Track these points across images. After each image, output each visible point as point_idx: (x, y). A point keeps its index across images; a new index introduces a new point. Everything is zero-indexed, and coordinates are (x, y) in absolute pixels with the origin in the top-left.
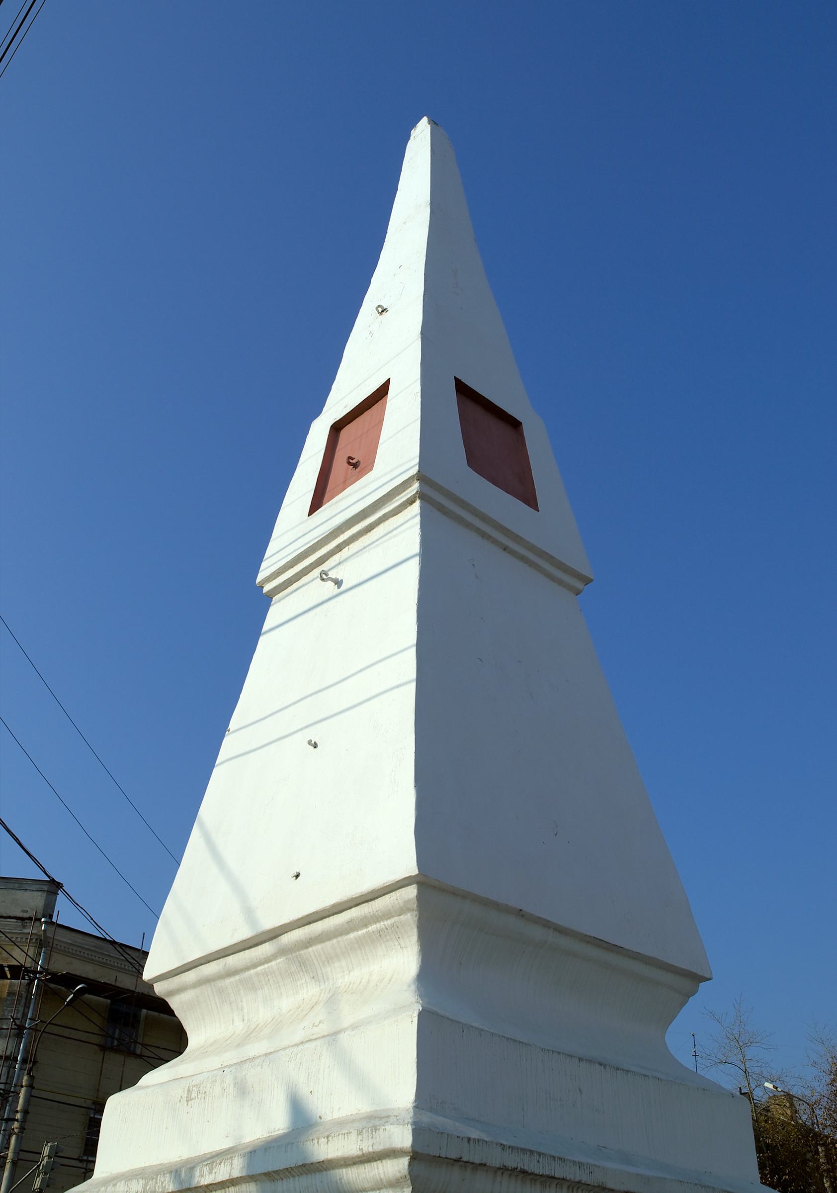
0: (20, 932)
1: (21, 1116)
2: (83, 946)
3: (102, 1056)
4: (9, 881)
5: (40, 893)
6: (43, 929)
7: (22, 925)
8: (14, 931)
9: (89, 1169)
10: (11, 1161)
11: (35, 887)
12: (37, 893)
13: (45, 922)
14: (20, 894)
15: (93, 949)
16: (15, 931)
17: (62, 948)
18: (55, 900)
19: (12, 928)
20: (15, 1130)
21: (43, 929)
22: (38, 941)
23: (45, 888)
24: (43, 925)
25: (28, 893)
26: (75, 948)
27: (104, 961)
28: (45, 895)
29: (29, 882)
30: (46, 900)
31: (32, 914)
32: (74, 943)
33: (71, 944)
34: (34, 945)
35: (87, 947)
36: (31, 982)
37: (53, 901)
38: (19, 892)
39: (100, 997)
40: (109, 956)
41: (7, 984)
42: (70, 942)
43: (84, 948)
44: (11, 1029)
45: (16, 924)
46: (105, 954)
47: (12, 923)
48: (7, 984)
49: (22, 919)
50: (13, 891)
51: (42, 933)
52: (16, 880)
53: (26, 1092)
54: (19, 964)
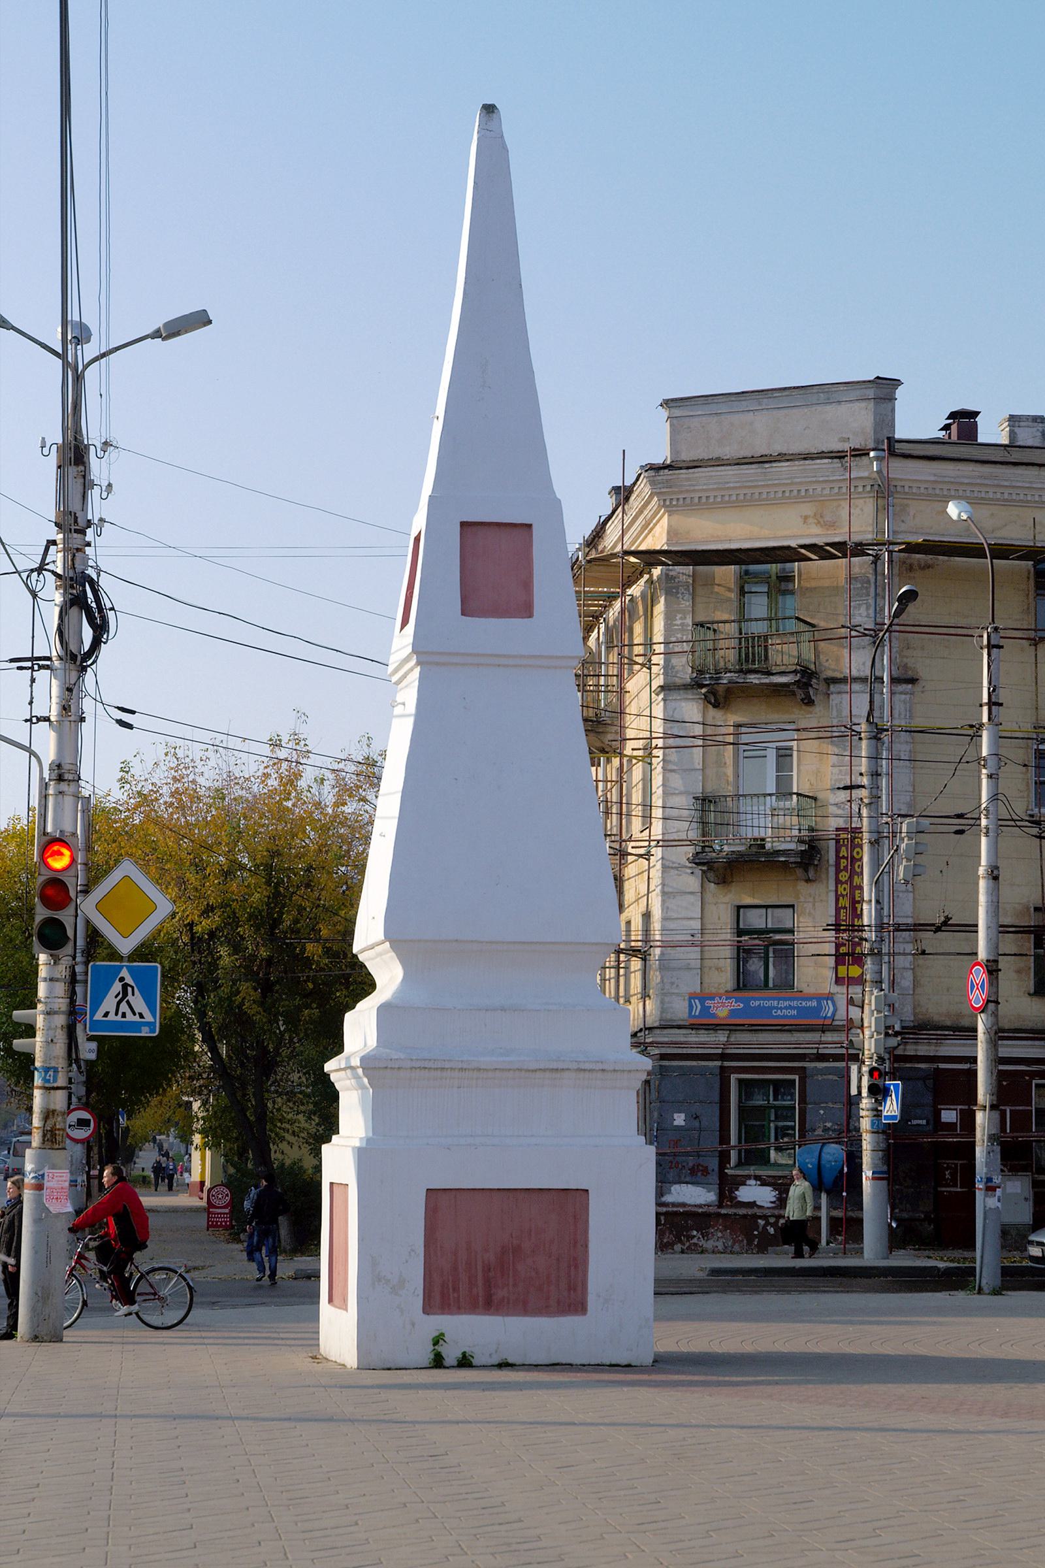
0: (842, 478)
1: (868, 781)
2: (958, 480)
3: (1034, 654)
4: (808, 392)
5: (863, 404)
6: (875, 469)
7: (842, 466)
8: (831, 479)
9: (649, 1056)
10: (867, 841)
11: (854, 394)
12: (858, 404)
13: (877, 458)
14: (830, 411)
15: (978, 481)
16: (834, 478)
17: (922, 490)
18: (893, 410)
19: (827, 474)
20: (864, 800)
21: (875, 469)
22: (876, 487)
23: (871, 393)
24: (875, 463)
25: (844, 408)
26: (945, 487)
27: (1006, 496)
28: (871, 405)
29: (842, 389)
30: (875, 414)
31: (856, 443)
32: (939, 479)
33: (935, 482)
34: (872, 495)
35: (966, 481)
36: (877, 558)
37: (890, 414)
38: (828, 407)
39: (1008, 559)
40: (1014, 487)
41: (842, 564)
42: (932, 478)
43: (962, 484)
44: (851, 637)
45: (832, 466)
46: (1006, 486)
47: (824, 466)
48: (842, 564)
49: (839, 456)
50: (819, 408)
51: (875, 475)
52: (818, 387)
53: (868, 746)
54: (627, 703)
